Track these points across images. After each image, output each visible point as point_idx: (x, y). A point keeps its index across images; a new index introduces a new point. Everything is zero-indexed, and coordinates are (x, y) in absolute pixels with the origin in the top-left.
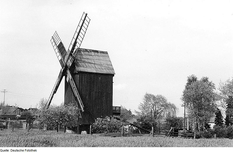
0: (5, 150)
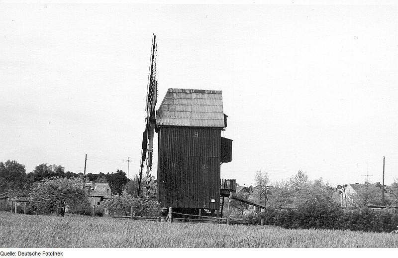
0: (8, 253)
